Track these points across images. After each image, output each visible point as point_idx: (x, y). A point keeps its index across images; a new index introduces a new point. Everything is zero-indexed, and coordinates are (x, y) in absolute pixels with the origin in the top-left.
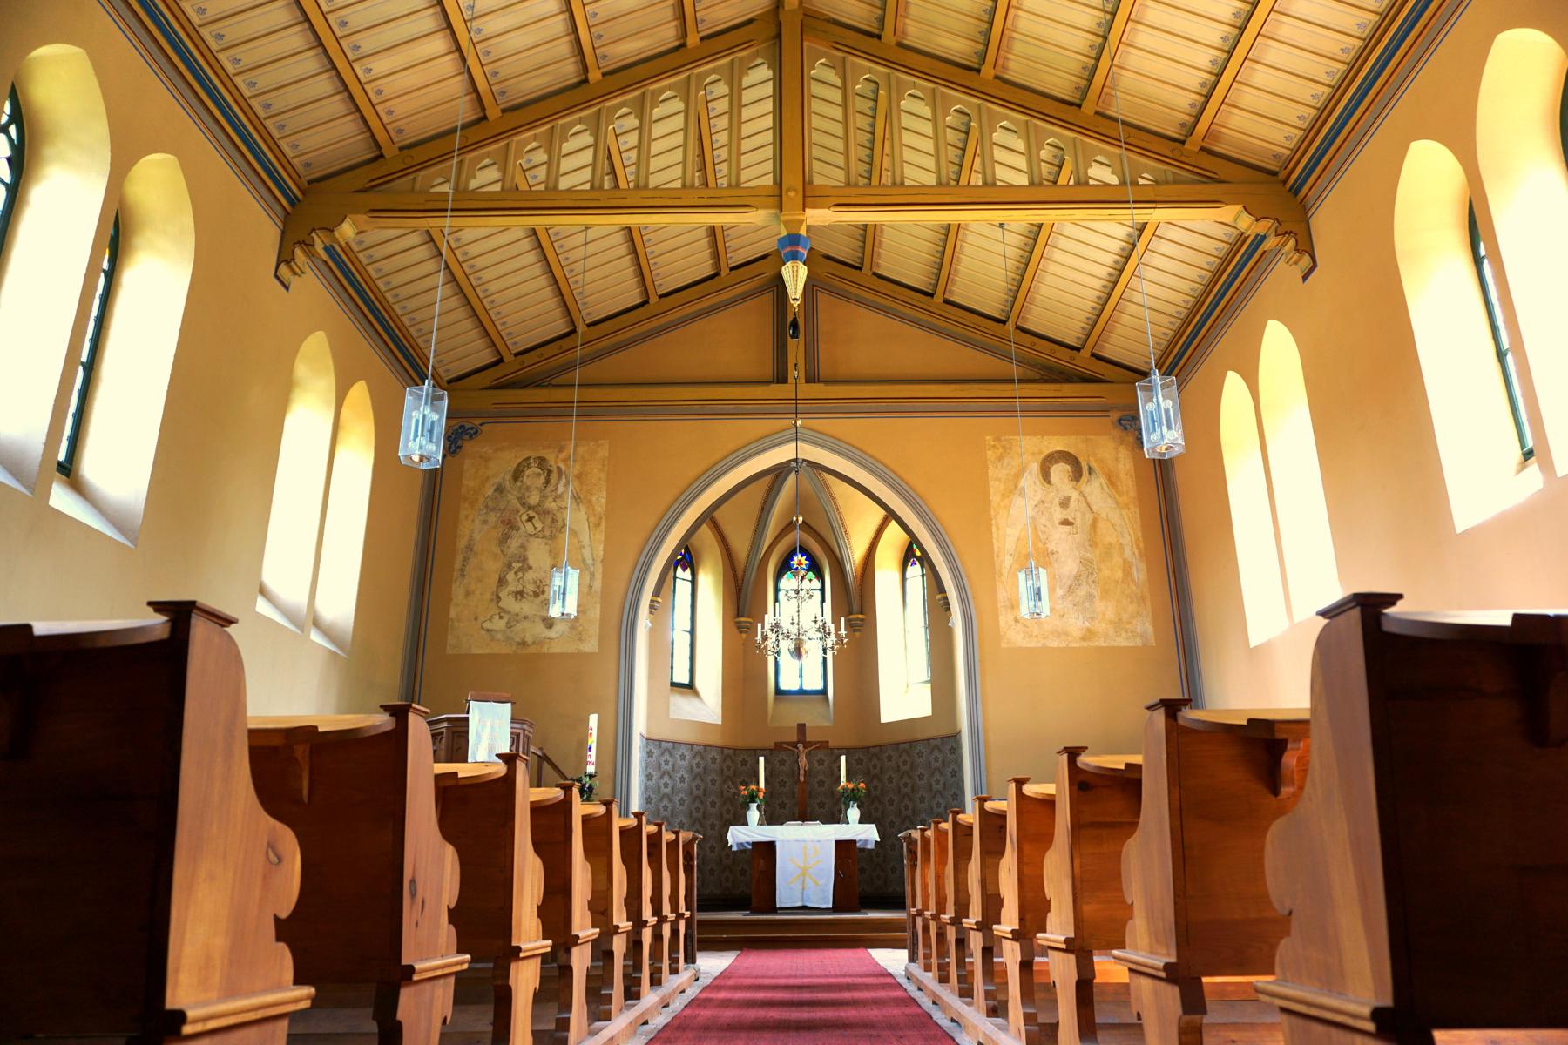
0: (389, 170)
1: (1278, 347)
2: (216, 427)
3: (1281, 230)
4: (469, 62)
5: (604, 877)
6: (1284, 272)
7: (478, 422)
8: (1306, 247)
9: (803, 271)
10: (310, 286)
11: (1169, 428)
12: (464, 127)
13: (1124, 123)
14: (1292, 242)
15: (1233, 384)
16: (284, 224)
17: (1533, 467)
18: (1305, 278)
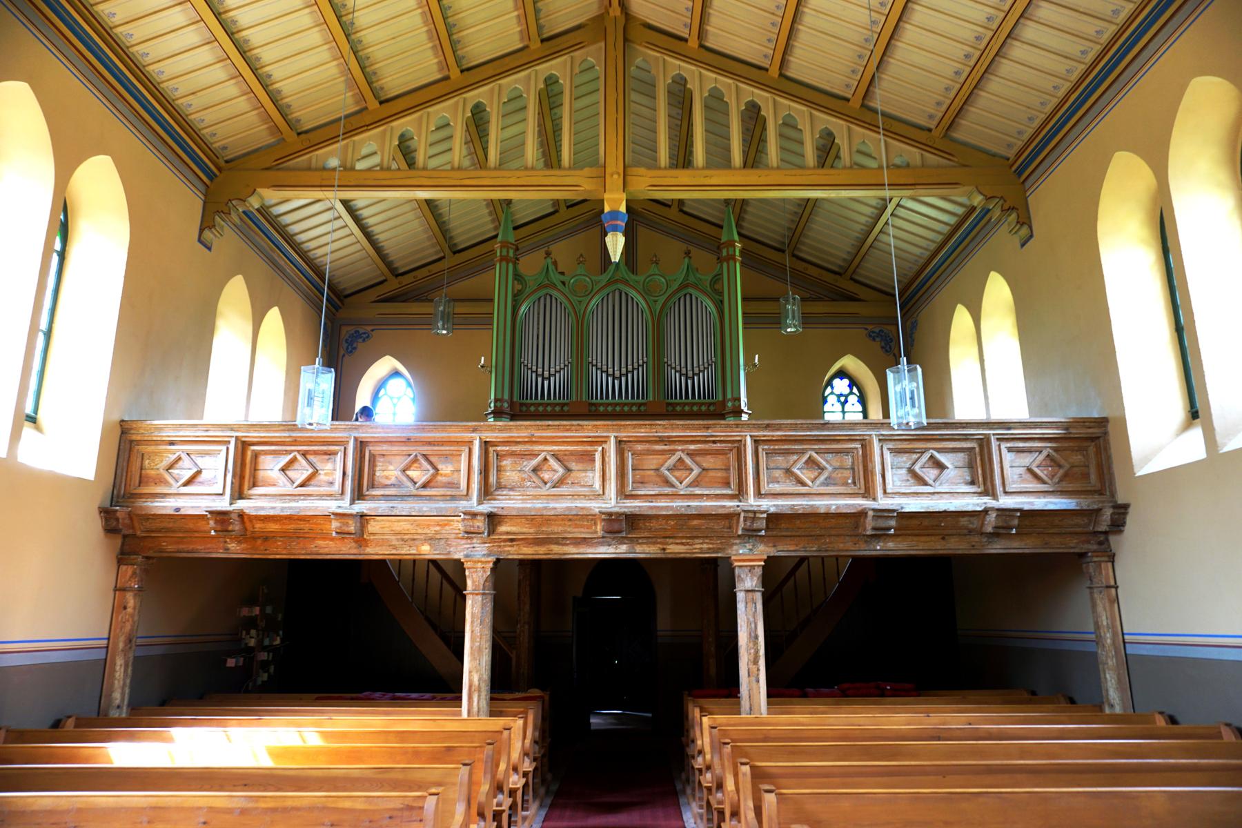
0: (291, 147)
1: (997, 291)
2: (160, 336)
3: (1006, 207)
4: (348, 46)
5: (480, 152)
6: (1003, 237)
7: (369, 328)
8: (1025, 221)
9: (621, 240)
10: (227, 239)
11: (913, 406)
12: (347, 117)
13: (884, 114)
14: (1014, 216)
15: (962, 318)
16: (205, 196)
17: (1197, 433)
18: (1023, 245)
